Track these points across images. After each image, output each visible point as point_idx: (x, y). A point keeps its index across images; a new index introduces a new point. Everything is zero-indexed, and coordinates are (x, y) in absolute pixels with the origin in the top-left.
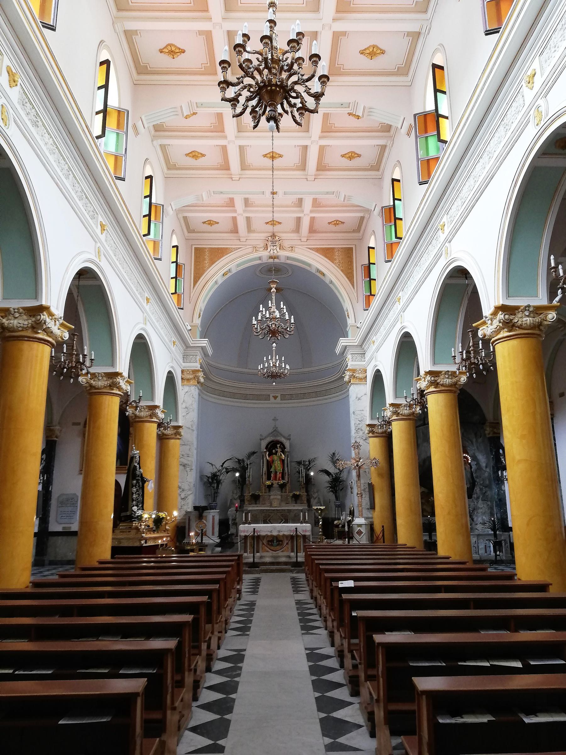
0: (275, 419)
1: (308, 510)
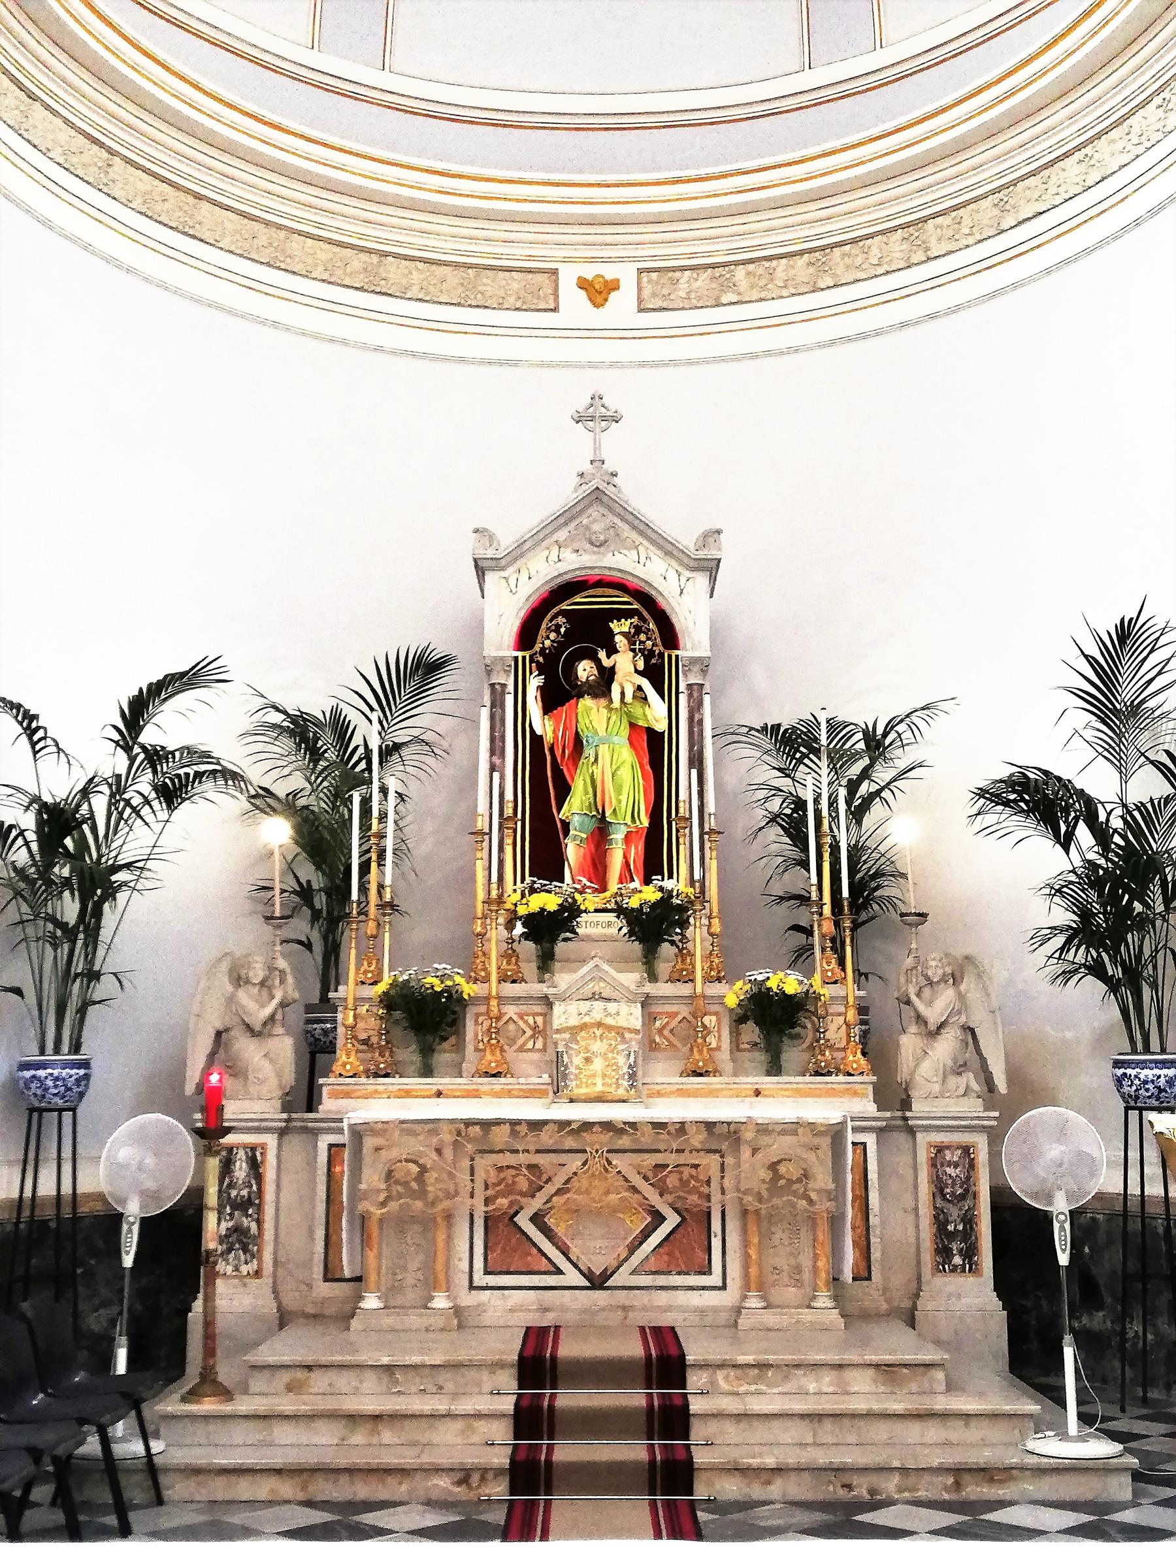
1: (880, 1131)
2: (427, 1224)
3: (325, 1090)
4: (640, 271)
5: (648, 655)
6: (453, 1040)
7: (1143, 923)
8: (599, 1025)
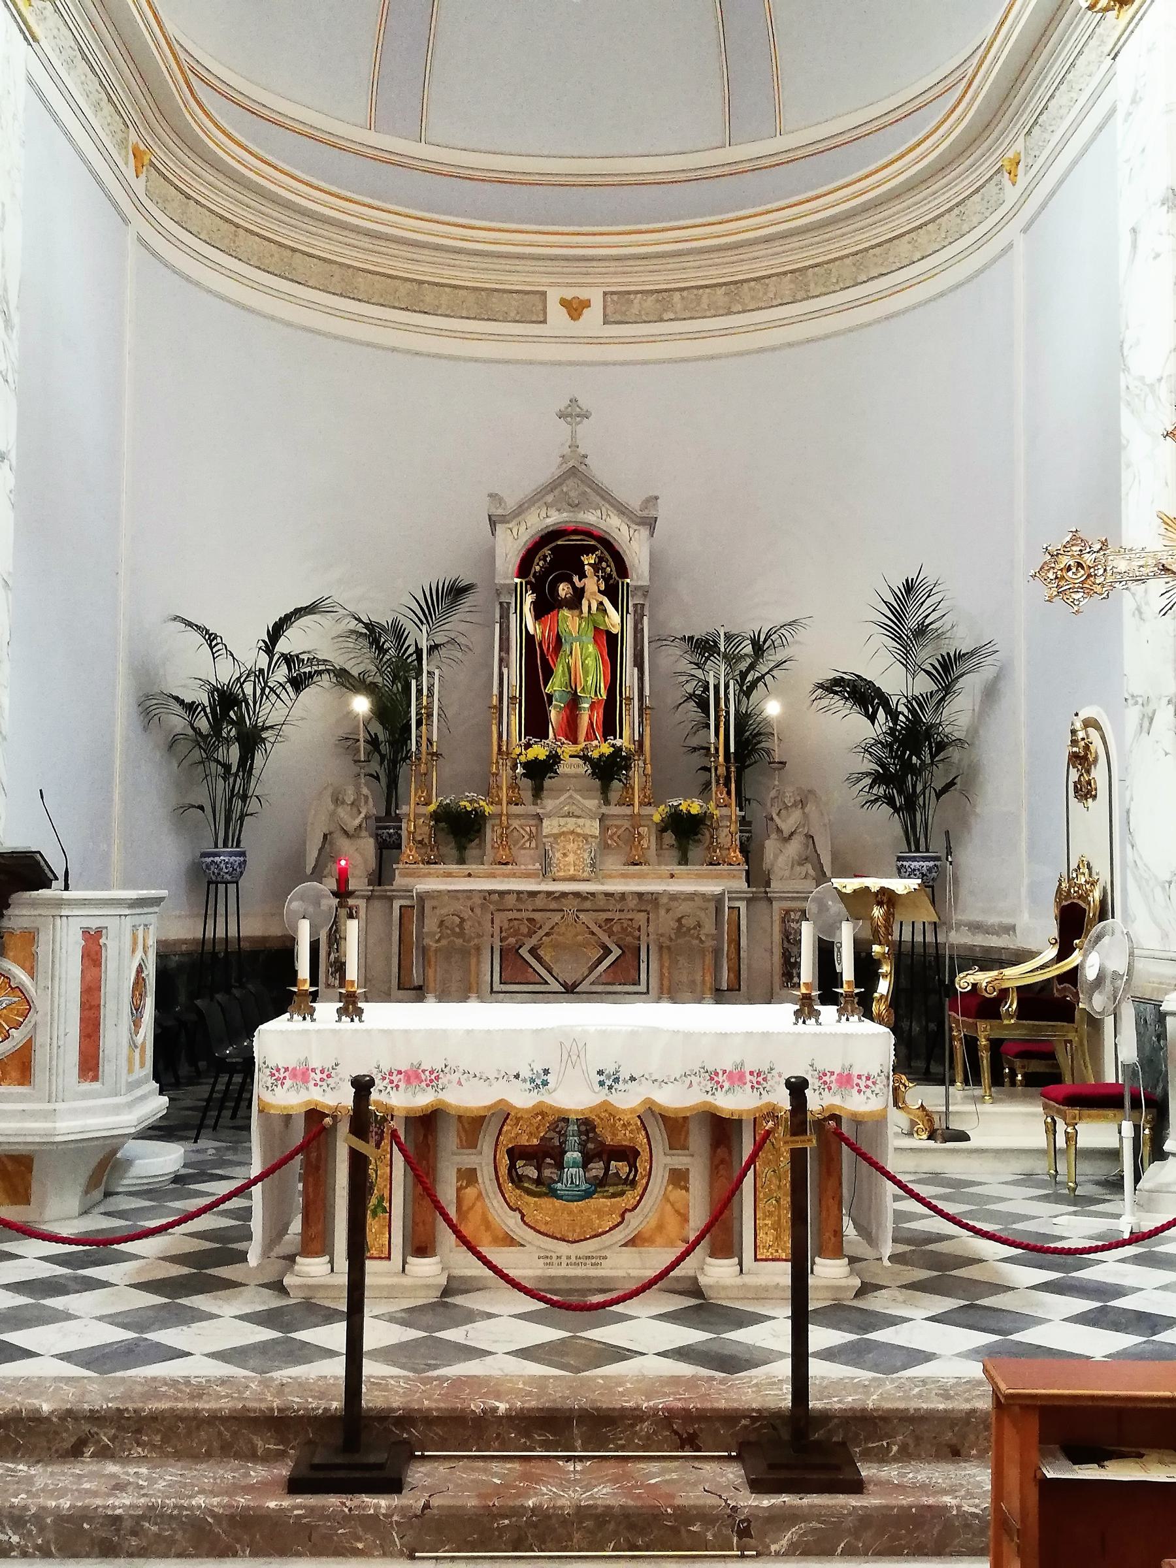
0: (573, 413)
2: (465, 953)
3: (397, 872)
4: (605, 294)
5: (607, 578)
6: (477, 841)
7: (916, 771)
8: (572, 832)
